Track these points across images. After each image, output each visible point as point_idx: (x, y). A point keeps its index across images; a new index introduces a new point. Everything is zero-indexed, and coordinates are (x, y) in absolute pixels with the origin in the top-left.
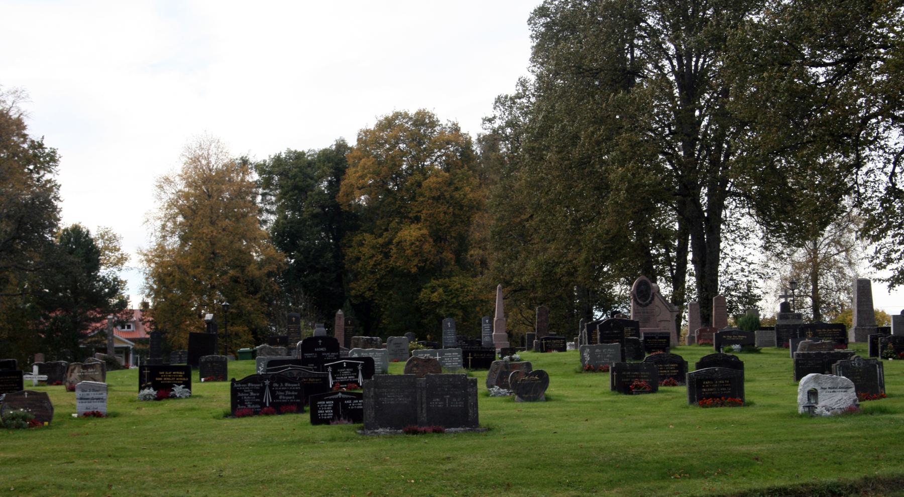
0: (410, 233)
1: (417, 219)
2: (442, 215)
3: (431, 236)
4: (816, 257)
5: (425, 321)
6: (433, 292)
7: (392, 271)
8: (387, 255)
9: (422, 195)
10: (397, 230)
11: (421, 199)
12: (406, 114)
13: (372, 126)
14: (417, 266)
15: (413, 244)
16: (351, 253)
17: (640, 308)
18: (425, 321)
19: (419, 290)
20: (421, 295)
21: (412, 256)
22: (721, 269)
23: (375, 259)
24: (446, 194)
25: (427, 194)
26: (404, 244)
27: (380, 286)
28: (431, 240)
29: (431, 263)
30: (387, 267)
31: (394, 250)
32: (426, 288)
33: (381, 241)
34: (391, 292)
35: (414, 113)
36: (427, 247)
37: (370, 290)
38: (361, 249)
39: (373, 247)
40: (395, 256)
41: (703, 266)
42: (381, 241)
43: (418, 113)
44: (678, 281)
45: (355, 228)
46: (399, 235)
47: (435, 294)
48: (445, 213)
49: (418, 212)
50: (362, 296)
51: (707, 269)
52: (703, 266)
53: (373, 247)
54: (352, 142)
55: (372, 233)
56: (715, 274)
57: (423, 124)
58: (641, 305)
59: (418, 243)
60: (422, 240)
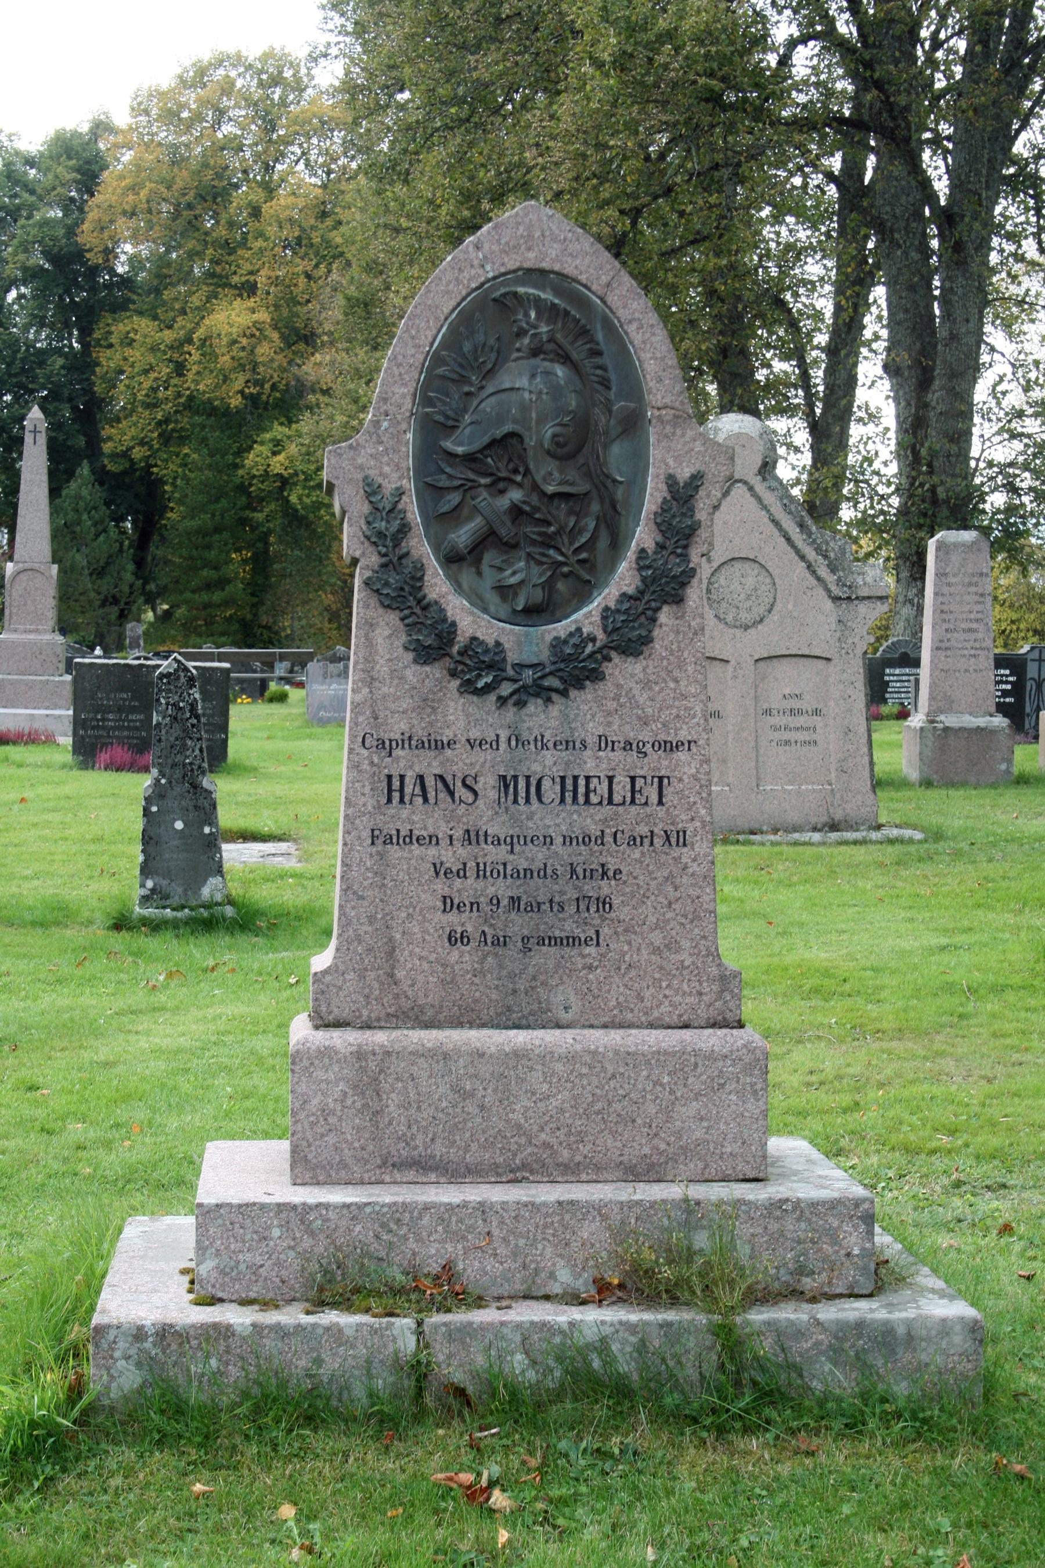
0: (231, 317)
1: (250, 289)
2: (302, 281)
3: (275, 328)
4: (608, 526)
5: (259, 516)
6: (275, 454)
7: (191, 404)
8: (180, 369)
9: (261, 235)
10: (204, 310)
11: (260, 243)
12: (239, 55)
13: (166, 81)
14: (242, 392)
15: (235, 342)
16: (108, 360)
17: (460, 715)
18: (259, 516)
19: (243, 451)
20: (250, 459)
21: (234, 369)
22: (981, 393)
23: (153, 375)
24: (314, 235)
25: (272, 230)
26: (215, 342)
27: (166, 439)
28: (275, 336)
29: (274, 387)
30: (179, 395)
31: (196, 356)
32: (262, 443)
33: (169, 336)
34: (186, 451)
35: (259, 54)
36: (264, 351)
37: (142, 443)
38: (128, 352)
39: (154, 349)
40: (195, 368)
41: (924, 383)
42: (169, 336)
43: (266, 56)
44: (829, 433)
45: (119, 307)
46: (207, 322)
47: (281, 458)
48: (309, 277)
49: (251, 273)
50: (125, 455)
51: (935, 396)
52: (924, 383)
53: (154, 349)
54: (122, 119)
55: (155, 318)
56: (961, 413)
57: (276, 81)
58: (478, 670)
59: (244, 341)
60: (255, 334)
